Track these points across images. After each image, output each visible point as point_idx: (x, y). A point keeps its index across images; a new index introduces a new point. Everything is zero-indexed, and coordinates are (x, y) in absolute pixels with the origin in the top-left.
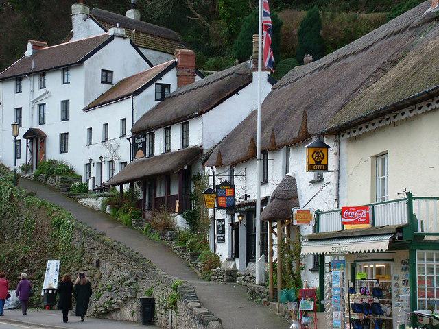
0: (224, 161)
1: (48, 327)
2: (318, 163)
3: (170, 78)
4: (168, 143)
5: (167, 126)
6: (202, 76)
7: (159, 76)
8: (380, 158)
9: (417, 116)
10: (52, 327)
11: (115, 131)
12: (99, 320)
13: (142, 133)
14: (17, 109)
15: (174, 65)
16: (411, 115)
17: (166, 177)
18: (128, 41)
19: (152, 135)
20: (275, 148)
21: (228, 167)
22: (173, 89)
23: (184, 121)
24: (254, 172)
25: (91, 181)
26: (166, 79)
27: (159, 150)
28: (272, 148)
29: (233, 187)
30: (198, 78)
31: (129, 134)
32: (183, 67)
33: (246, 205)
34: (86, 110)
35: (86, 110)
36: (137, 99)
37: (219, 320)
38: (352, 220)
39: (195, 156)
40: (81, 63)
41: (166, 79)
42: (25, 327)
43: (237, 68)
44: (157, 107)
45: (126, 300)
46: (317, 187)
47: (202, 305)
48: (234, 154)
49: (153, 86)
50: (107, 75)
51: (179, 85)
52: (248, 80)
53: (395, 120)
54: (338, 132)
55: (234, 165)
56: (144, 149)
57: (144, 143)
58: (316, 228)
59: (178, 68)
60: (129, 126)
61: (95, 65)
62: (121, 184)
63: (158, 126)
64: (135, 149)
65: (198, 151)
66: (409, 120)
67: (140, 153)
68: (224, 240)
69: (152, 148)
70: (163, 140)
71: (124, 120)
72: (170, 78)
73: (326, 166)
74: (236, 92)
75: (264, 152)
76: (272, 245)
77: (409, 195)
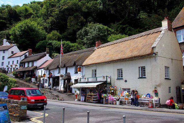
3: (27, 54)
7: (25, 53)
11: (15, 63)
13: (22, 64)
14: (3, 56)
15: (28, 52)
18: (17, 47)
22: (28, 56)
24: (57, 71)
25: (9, 71)
26: (26, 54)
30: (32, 55)
34: (8, 58)
35: (8, 58)
38: (35, 94)
39: (36, 68)
40: (8, 50)
41: (26, 54)
43: (43, 53)
49: (14, 53)
50: (12, 52)
51: (29, 55)
52: (46, 55)
56: (22, 66)
57: (23, 65)
58: (80, 81)
59: (29, 52)
61: (10, 50)
63: (27, 62)
68: (47, 83)
71: (18, 61)
72: (27, 54)
74: (43, 57)
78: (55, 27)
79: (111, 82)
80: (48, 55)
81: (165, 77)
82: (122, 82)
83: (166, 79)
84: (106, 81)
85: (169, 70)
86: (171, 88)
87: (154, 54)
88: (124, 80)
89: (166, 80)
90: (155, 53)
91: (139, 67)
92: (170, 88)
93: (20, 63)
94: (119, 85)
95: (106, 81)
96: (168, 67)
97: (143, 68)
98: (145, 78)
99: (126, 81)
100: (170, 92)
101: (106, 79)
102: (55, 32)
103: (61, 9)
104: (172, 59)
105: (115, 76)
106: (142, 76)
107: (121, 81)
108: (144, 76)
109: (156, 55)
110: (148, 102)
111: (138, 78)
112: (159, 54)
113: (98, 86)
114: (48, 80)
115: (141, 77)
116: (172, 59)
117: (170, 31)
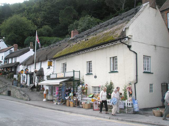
0: (26, 64)
1: (154, 125)
2: (50, 65)
4: (12, 61)
5: (12, 58)
6: (19, 49)
7: (10, 49)
8: (65, 65)
9: (63, 59)
10: (157, 125)
12: (8, 96)
13: (7, 59)
16: (87, 52)
17: (11, 67)
19: (9, 59)
20: (38, 62)
21: (26, 66)
23: (16, 57)
26: (11, 49)
27: (10, 62)
28: (38, 61)
29: (28, 69)
30: (18, 50)
31: (4, 59)
32: (15, 47)
33: (30, 73)
36: (6, 52)
37: (28, 95)
39: (18, 64)
42: (128, 123)
44: (9, 54)
45: (4, 91)
46: (49, 70)
47: (24, 92)
48: (29, 62)
49: (9, 50)
52: (29, 50)
53: (69, 56)
54: (55, 59)
55: (28, 65)
56: (7, 62)
60: (4, 58)
62: (1, 69)
64: (5, 62)
65: (19, 63)
66: (72, 56)
67: (6, 63)
69: (8, 62)
70: (11, 61)
73: (52, 65)
75: (36, 63)
76: (35, 82)
77: (74, 71)
78: (48, 22)
79: (80, 79)
80: (31, 50)
81: (143, 71)
82: (92, 77)
83: (144, 72)
84: (72, 77)
85: (151, 61)
86: (153, 85)
87: (127, 39)
88: (94, 75)
89: (145, 74)
90: (128, 37)
91: (111, 58)
92: (151, 85)
93: (4, 58)
94: (90, 82)
95: (73, 77)
96: (150, 57)
97: (116, 58)
98: (117, 72)
99: (95, 77)
100: (151, 91)
101: (22, 68)
102: (47, 27)
103: (54, 2)
104: (155, 46)
105: (84, 71)
106: (113, 69)
107: (91, 76)
108: (116, 69)
109: (131, 40)
110: (130, 106)
111: (109, 73)
112: (133, 38)
113: (61, 83)
114: (26, 76)
115: (112, 70)
116: (155, 46)
117: (153, 8)
